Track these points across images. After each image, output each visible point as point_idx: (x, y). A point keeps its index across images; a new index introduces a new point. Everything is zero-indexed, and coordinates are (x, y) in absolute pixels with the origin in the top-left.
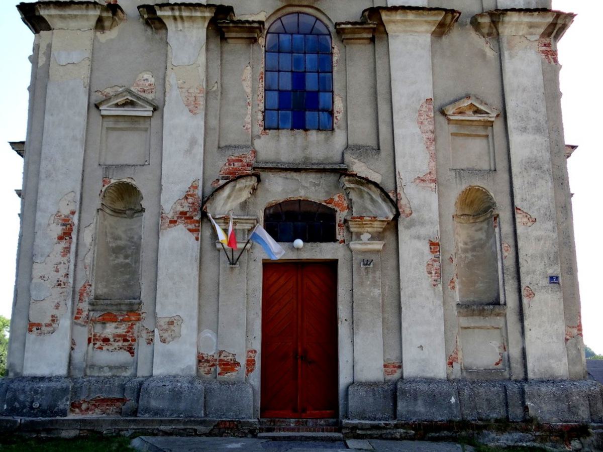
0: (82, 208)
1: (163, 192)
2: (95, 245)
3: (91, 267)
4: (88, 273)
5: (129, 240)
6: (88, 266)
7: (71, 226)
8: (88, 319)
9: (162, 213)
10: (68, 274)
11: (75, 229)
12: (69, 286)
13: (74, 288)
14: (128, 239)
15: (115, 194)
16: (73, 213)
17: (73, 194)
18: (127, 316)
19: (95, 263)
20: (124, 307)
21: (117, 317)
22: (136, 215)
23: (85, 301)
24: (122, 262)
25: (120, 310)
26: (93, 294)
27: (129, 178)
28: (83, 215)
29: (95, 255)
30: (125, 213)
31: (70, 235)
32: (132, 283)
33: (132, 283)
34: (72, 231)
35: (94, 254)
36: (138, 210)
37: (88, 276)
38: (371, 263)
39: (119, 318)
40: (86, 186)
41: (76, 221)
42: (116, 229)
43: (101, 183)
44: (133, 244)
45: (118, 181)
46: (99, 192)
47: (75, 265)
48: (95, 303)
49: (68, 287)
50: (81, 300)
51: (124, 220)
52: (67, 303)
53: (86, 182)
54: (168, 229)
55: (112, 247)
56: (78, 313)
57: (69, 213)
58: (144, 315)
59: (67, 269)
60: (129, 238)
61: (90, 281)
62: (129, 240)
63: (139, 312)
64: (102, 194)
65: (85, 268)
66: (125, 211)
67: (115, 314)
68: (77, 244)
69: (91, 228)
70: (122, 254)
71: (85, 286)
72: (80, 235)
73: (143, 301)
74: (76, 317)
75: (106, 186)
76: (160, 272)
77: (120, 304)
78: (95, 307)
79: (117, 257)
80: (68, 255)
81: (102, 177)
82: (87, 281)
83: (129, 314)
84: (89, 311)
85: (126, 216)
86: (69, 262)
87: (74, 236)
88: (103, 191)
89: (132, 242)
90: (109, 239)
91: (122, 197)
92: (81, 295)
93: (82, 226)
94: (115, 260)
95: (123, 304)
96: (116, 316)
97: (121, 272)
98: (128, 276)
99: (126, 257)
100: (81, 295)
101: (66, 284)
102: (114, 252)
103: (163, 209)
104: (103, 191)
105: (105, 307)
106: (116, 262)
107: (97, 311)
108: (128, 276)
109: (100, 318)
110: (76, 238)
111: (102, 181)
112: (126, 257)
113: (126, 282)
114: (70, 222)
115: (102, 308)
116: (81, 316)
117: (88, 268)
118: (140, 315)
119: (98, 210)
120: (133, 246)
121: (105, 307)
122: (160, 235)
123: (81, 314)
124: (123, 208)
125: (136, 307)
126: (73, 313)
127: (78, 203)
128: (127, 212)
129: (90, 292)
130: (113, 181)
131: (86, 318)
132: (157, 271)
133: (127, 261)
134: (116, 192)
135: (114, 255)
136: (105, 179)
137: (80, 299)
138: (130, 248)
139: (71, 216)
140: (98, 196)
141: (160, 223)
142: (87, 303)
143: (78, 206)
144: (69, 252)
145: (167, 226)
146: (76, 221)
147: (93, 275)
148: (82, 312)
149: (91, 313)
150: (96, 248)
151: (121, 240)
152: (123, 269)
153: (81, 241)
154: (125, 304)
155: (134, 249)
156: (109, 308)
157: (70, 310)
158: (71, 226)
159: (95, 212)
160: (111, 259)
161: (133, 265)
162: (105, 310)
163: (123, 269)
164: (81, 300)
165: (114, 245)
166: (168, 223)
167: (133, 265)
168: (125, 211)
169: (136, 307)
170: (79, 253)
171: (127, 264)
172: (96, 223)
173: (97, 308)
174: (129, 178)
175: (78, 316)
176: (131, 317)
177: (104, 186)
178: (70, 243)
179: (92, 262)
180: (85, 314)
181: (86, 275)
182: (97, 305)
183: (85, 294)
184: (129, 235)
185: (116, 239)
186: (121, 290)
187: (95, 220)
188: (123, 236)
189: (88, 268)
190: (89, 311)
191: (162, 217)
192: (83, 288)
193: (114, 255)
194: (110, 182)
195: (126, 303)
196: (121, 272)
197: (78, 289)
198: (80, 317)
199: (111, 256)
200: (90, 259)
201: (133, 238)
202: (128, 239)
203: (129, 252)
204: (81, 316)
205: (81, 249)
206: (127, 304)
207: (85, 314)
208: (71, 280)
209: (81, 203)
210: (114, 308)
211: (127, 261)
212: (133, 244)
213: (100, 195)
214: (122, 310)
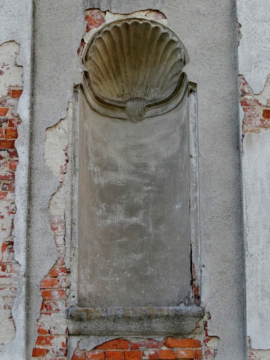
0: (37, 82)
1: (244, 41)
2: (74, 171)
3: (68, 227)
4: (60, 240)
5: (134, 172)
6: (60, 222)
7: (11, 125)
8: (66, 355)
9: (244, 93)
10: (12, 243)
11: (23, 131)
12: (18, 273)
13: (27, 275)
14: (133, 168)
15: (105, 58)
16: (16, 93)
17: (14, 48)
18: (164, 348)
19: (76, 217)
20: (158, 326)
21: (141, 348)
22: (150, 112)
23: (58, 310)
24: (121, 224)
25: (149, 333)
26: (75, 293)
27: (151, 10)
28: (39, 98)
29: (76, 197)
30: (123, 108)
31: (13, 146)
32: (150, 271)
33: (150, 271)
34: (16, 137)
35: (72, 194)
36: (154, 99)
37: (62, 248)
38: (204, 313)
39: (147, 353)
40: (43, 30)
41: (24, 113)
42: (105, 144)
43: (81, 24)
44: (147, 181)
45: (123, 17)
46: (78, 44)
47: (29, 222)
48: (84, 315)
49: (15, 275)
50: (46, 308)
51: (118, 124)
52: (13, 315)
53: (42, 20)
54: (263, 130)
55: (99, 185)
56: (40, 340)
57: (5, 93)
58: (212, 344)
59: (8, 230)
60: (136, 166)
61: (66, 262)
62: (134, 172)
63: (196, 338)
64: (84, 51)
65: (54, 229)
66: (125, 103)
67: (134, 341)
68: (30, 169)
69: (61, 131)
70: (121, 204)
71: (53, 274)
72: (35, 148)
73: (207, 310)
74: (35, 349)
75: (94, 30)
76: (250, 237)
77: (149, 317)
78: (83, 325)
79: (109, 210)
80: (9, 195)
81: (81, 8)
82: (60, 261)
83: (170, 341)
84: (69, 334)
85: (123, 115)
86: (13, 212)
87: (22, 149)
88: (87, 41)
89: (144, 176)
90: (92, 167)
91: (118, 68)
92: (46, 294)
93: (40, 126)
94: (105, 218)
95: (157, 317)
96: (136, 347)
97: (121, 246)
98: (139, 257)
99: (131, 211)
100: (46, 294)
101: (8, 268)
102: (103, 198)
103: (245, 83)
104: (87, 41)
105: (110, 325)
106: (109, 221)
107: (88, 335)
108: (139, 257)
109: (97, 352)
110: (27, 153)
111: (83, 19)
112: (131, 211)
113: (135, 270)
114: (9, 116)
115: (102, 326)
116: (48, 347)
117: (60, 229)
118: (198, 344)
119: (75, 87)
120: (147, 185)
121: (110, 325)
122: (244, 145)
123: (48, 343)
124: (118, 96)
125: (189, 325)
126: (27, 342)
127: (28, 69)
128: (129, 105)
129: (68, 287)
130: (110, 18)
131: (63, 353)
132: (240, 235)
133: (134, 220)
134: (107, 53)
135: (103, 206)
136: (88, 13)
137: (44, 306)
138: (138, 190)
139: (11, 101)
140: (76, 53)
141: (241, 118)
142: (62, 314)
143: (27, 77)
144: (13, 190)
145: (258, 123)
146: (24, 113)
147: (72, 247)
148: (51, 338)
149: (74, 340)
150: (76, 179)
151: (116, 170)
152: (125, 239)
153: (36, 164)
154: (162, 316)
155: (151, 191)
156: (121, 327)
157: (21, 332)
158: (11, 125)
159: (70, 93)
160: (99, 213)
161: (151, 229)
162: (109, 333)
163: (125, 239)
164: (46, 308)
165: (102, 181)
166: (261, 117)
167: (151, 229)
168: (125, 103)
169: (189, 325)
170: (35, 191)
171: (136, 227)
172: (74, 119)
173: (90, 326)
174: (151, 10)
175: (41, 347)
176: (175, 350)
177: (88, 29)
178: (13, 168)
179: (68, 213)
180: (58, 342)
181: (57, 246)
182: (89, 319)
183: (55, 293)
184: (135, 160)
185: (105, 169)
186: (123, 289)
187: (71, 111)
188: (121, 162)
189: (60, 229)
190: (69, 335)
191: (244, 103)
192: (49, 278)
193: (103, 206)
194: (103, 20)
195: (166, 313)
196: (121, 246)
197: (36, 281)
198: (48, 351)
199: (99, 207)
200: (63, 207)
201: (145, 166)
202: (133, 168)
203: (138, 199)
204: (48, 347)
205: (39, 182)
206: (167, 317)
207: (58, 342)
208: (21, 257)
209: (34, 71)
210: (134, 326)
211: (134, 220)
212: (147, 181)
213: (79, 51)
214: (155, 333)
